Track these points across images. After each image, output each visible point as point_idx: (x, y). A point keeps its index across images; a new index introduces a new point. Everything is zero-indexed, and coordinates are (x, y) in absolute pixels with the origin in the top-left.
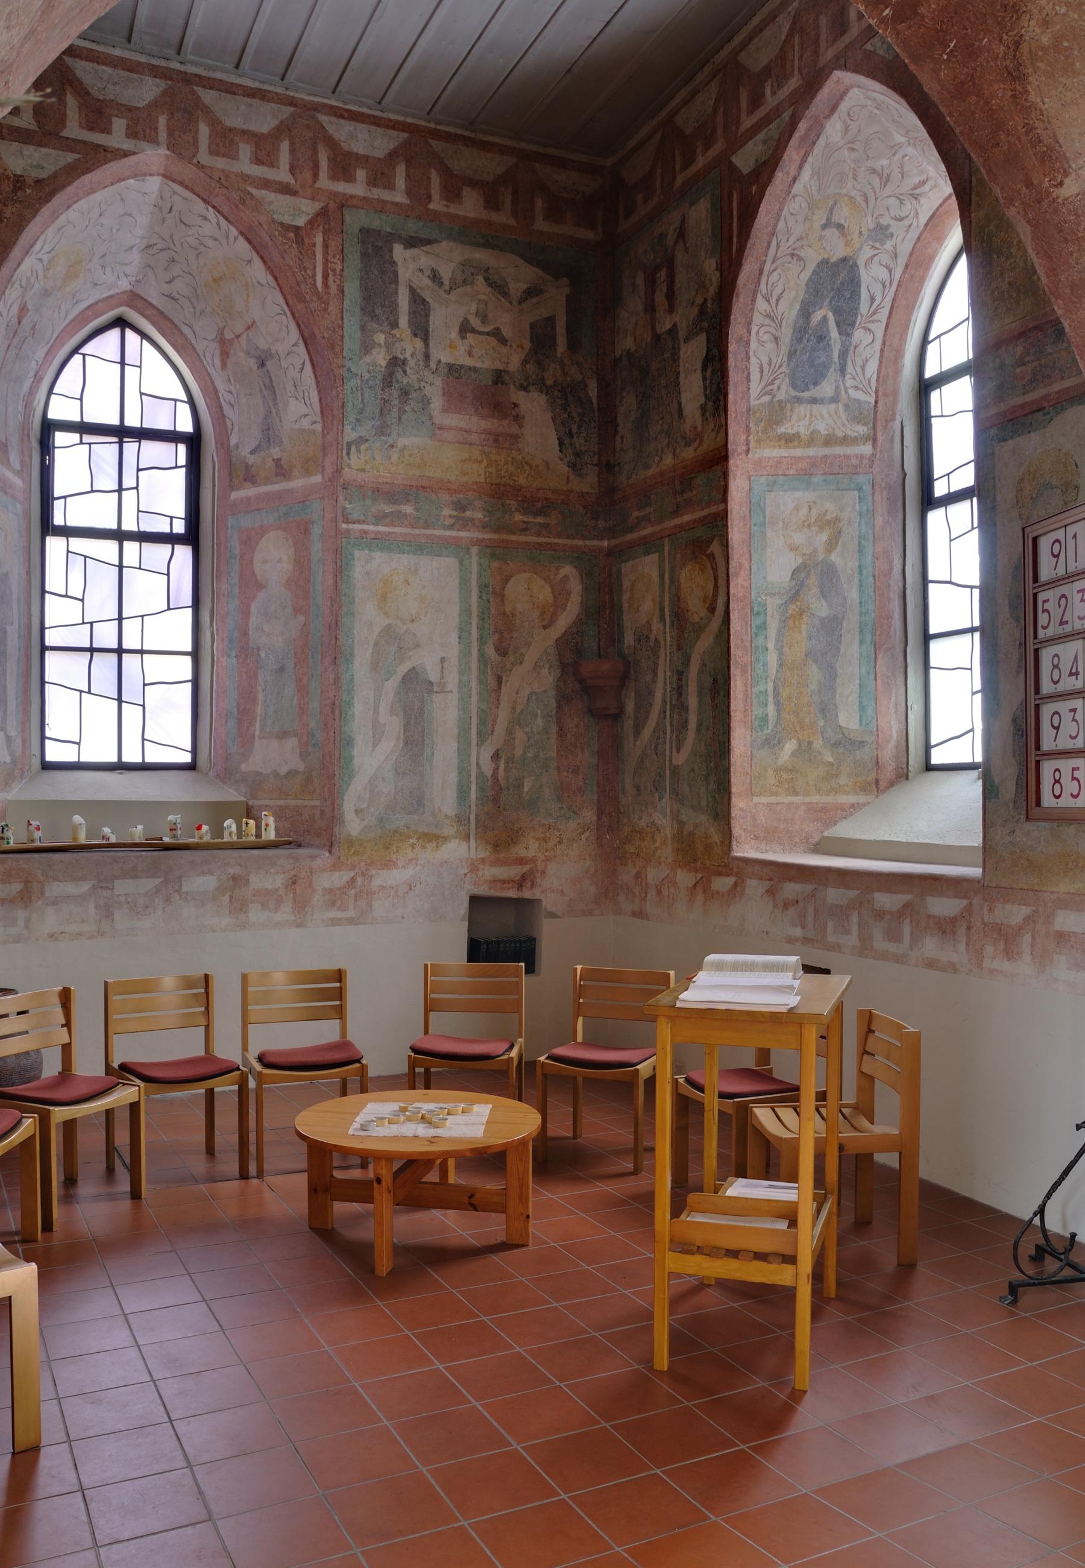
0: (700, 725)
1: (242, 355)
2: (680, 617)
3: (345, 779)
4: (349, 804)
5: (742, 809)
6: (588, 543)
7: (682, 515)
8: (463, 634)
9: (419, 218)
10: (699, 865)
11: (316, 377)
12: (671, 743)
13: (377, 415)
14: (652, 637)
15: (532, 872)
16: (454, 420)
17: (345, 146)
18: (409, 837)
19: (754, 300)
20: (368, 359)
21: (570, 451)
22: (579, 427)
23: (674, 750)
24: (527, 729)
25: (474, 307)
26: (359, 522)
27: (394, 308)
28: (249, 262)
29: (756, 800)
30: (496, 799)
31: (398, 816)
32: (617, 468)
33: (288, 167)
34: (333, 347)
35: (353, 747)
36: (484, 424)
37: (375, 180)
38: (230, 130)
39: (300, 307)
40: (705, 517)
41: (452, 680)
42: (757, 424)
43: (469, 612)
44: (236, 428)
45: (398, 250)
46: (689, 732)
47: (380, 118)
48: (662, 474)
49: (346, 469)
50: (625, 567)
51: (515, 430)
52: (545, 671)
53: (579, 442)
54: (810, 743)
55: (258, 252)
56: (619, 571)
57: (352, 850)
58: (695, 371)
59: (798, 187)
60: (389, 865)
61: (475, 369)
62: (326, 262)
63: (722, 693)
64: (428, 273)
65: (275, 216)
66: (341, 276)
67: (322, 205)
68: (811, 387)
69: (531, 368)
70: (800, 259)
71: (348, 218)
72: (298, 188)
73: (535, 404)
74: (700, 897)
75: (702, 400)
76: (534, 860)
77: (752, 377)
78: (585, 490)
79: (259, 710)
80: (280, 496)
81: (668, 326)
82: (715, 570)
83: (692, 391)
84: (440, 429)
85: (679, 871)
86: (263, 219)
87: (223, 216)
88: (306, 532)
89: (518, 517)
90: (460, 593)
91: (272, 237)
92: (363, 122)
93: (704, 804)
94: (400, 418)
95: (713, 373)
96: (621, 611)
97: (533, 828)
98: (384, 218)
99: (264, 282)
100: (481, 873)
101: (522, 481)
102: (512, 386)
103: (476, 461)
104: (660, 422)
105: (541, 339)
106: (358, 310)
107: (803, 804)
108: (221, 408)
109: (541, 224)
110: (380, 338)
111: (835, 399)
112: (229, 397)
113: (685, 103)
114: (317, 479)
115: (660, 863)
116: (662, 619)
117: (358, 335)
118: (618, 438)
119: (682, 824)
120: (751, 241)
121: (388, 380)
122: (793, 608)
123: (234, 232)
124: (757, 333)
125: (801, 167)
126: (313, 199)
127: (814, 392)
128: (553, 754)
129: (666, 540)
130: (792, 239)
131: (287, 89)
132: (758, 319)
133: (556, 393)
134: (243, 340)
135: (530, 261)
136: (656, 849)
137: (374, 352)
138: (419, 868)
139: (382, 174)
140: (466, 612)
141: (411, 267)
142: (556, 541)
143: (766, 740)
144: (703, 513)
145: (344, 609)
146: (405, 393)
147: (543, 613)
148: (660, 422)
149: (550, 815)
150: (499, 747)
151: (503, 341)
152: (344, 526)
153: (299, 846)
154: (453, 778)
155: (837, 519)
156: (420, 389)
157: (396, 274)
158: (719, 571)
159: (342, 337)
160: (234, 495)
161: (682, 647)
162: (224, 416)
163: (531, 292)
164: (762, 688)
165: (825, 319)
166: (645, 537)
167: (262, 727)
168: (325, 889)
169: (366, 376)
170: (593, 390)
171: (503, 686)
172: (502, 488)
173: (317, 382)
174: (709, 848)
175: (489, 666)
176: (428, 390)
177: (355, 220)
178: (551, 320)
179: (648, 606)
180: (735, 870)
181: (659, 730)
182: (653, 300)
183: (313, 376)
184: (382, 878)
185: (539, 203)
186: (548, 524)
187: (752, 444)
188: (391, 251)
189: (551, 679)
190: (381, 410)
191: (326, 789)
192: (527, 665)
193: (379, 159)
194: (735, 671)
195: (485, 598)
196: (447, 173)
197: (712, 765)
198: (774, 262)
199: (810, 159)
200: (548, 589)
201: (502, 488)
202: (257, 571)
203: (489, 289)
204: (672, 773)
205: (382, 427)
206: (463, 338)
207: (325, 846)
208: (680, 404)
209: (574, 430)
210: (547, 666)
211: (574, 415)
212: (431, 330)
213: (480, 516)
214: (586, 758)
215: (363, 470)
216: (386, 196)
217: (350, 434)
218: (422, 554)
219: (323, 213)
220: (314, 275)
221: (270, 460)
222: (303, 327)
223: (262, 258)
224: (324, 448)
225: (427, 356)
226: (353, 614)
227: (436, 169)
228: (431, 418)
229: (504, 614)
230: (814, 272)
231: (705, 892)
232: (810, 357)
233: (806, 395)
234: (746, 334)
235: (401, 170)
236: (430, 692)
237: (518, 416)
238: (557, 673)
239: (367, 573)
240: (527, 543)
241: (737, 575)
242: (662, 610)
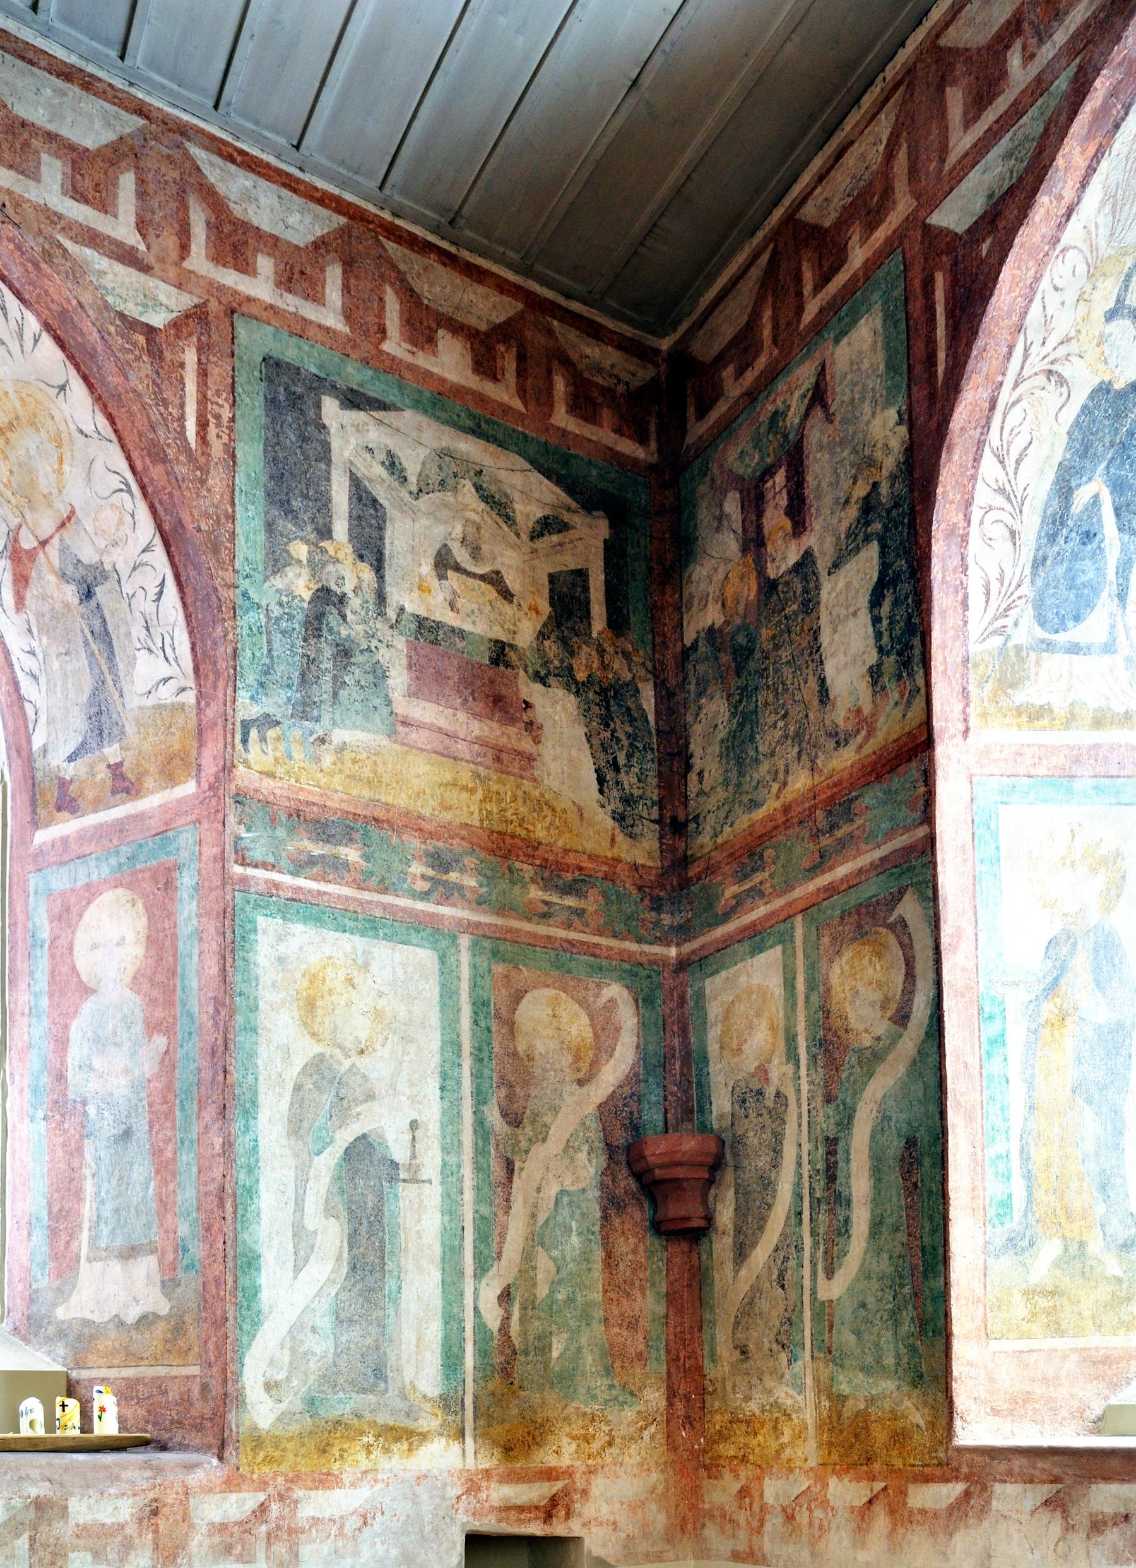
0: (876, 1226)
1: (52, 578)
2: (830, 1045)
3: (246, 1327)
4: (253, 1372)
5: (970, 1364)
6: (646, 948)
7: (831, 869)
8: (447, 1084)
9: (366, 362)
10: (877, 1466)
11: (185, 605)
12: (814, 1264)
13: (296, 681)
14: (770, 1092)
15: (566, 1492)
16: (426, 712)
17: (237, 210)
18: (362, 1433)
19: (977, 460)
20: (278, 582)
21: (615, 793)
22: (629, 756)
23: (821, 1275)
24: (555, 1253)
25: (458, 530)
26: (264, 865)
27: (323, 504)
28: (62, 388)
29: (994, 1345)
30: (506, 1371)
31: (341, 1395)
32: (692, 826)
33: (132, 219)
34: (216, 550)
35: (258, 1269)
36: (477, 728)
37: (290, 280)
38: (23, 124)
39: (156, 472)
40: (883, 859)
41: (431, 1161)
42: (980, 686)
43: (456, 1045)
44: (43, 719)
45: (330, 407)
46: (854, 1241)
47: (298, 181)
48: (786, 809)
49: (241, 768)
50: (713, 985)
51: (527, 745)
52: (582, 1156)
53: (629, 780)
54: (1082, 1245)
55: (77, 367)
56: (700, 995)
57: (262, 1455)
58: (855, 614)
59: (1073, 232)
60: (326, 1481)
61: (462, 634)
62: (203, 400)
63: (927, 1162)
64: (382, 457)
65: (110, 299)
66: (231, 429)
67: (196, 301)
68: (1070, 624)
69: (551, 647)
70: (1062, 381)
71: (243, 331)
72: (151, 260)
73: (559, 708)
74: (881, 1521)
75: (873, 658)
76: (569, 1473)
77: (971, 602)
78: (640, 861)
79: (87, 1210)
80: (121, 827)
81: (793, 558)
82: (907, 947)
83: (848, 646)
84: (404, 723)
85: (833, 1481)
86: (86, 298)
87: (11, 287)
88: (169, 886)
89: (536, 893)
90: (442, 1011)
91: (103, 335)
92: (268, 178)
93: (889, 1361)
94: (335, 695)
95: (896, 603)
96: (705, 1060)
97: (567, 1419)
98: (306, 348)
99: (89, 428)
100: (484, 1495)
101: (540, 834)
102: (522, 672)
103: (465, 788)
104: (781, 724)
105: (566, 601)
106: (260, 493)
107: (1074, 1350)
108: (16, 685)
109: (562, 418)
110: (300, 550)
111: (1109, 648)
112: (30, 663)
113: (821, 178)
114: (189, 788)
115: (791, 1470)
116: (792, 1055)
117: (261, 537)
118: (693, 777)
119: (839, 1400)
120: (980, 343)
121: (314, 625)
122: (1048, 1009)
123: (33, 324)
124: (981, 523)
125: (1084, 184)
126: (179, 286)
127: (1075, 634)
128: (598, 1296)
129: (799, 921)
130: (1052, 341)
131: (131, 84)
132: (983, 495)
133: (591, 695)
134: (53, 550)
135: (548, 474)
136: (782, 1446)
137: (291, 572)
138: (379, 1486)
139: (302, 273)
140: (452, 1044)
141: (353, 441)
142: (596, 939)
143: (1010, 1240)
144: (878, 854)
145: (239, 1018)
146: (344, 653)
147: (577, 1058)
148: (781, 724)
149: (594, 1397)
150: (510, 1281)
151: (507, 595)
152: (238, 869)
153: (164, 1448)
154: (434, 1331)
155: (1118, 855)
156: (369, 650)
157: (326, 447)
158: (917, 946)
159: (233, 535)
160: (42, 837)
161: (836, 1096)
162: (21, 699)
163: (547, 526)
164: (1000, 1148)
165: (1096, 500)
166: (753, 925)
167: (93, 1241)
168: (212, 1524)
169: (276, 611)
170: (648, 699)
171: (515, 1178)
172: (508, 840)
173: (188, 617)
174: (900, 1437)
175: (492, 1142)
176: (383, 655)
177: (256, 341)
178: (581, 575)
179: (760, 1039)
180: (965, 1469)
181: (788, 1246)
182: (759, 528)
183: (179, 605)
184: (315, 1504)
185: (560, 385)
186: (584, 911)
187: (973, 721)
188: (318, 406)
189: (592, 1171)
190: (303, 675)
191: (211, 1346)
192: (554, 1145)
193: (297, 247)
194: (954, 1118)
195: (483, 1024)
196: (410, 297)
197: (907, 1290)
198: (1016, 385)
199: (1104, 166)
200: (585, 1020)
201: (508, 840)
202: (82, 965)
203: (483, 505)
204: (817, 1317)
205: (304, 704)
206: (442, 577)
207: (210, 1447)
208: (822, 681)
209: (622, 761)
210: (586, 1147)
211: (620, 734)
212: (387, 553)
213: (473, 883)
214: (650, 1305)
215: (271, 775)
216: (309, 311)
217: (247, 707)
218: (377, 937)
219: (197, 316)
220: (182, 418)
221: (102, 767)
222: (162, 513)
223: (85, 378)
224: (200, 731)
225: (381, 598)
226: (254, 1030)
227: (392, 285)
228: (389, 702)
229: (515, 1054)
230: (1085, 407)
231: (892, 1512)
232: (1069, 569)
233: (1061, 638)
234: (963, 524)
235: (334, 276)
236: (393, 1179)
237: (531, 723)
238: (602, 1160)
239: (281, 960)
240: (549, 937)
241: (955, 948)
242: (791, 1040)
